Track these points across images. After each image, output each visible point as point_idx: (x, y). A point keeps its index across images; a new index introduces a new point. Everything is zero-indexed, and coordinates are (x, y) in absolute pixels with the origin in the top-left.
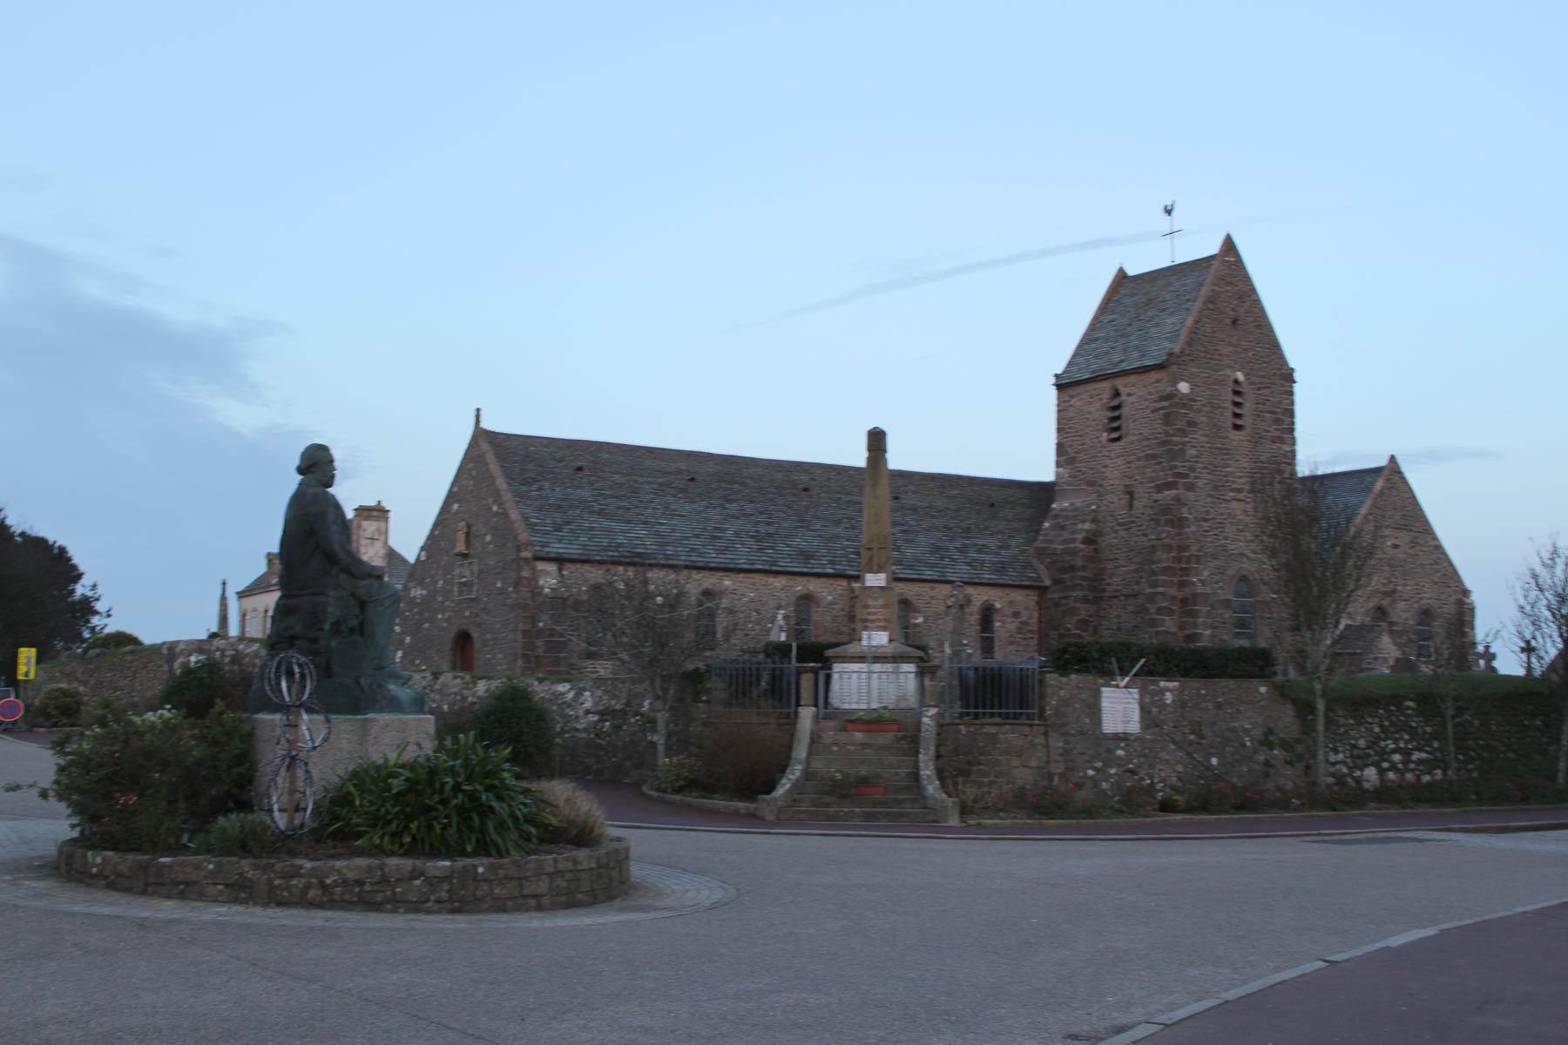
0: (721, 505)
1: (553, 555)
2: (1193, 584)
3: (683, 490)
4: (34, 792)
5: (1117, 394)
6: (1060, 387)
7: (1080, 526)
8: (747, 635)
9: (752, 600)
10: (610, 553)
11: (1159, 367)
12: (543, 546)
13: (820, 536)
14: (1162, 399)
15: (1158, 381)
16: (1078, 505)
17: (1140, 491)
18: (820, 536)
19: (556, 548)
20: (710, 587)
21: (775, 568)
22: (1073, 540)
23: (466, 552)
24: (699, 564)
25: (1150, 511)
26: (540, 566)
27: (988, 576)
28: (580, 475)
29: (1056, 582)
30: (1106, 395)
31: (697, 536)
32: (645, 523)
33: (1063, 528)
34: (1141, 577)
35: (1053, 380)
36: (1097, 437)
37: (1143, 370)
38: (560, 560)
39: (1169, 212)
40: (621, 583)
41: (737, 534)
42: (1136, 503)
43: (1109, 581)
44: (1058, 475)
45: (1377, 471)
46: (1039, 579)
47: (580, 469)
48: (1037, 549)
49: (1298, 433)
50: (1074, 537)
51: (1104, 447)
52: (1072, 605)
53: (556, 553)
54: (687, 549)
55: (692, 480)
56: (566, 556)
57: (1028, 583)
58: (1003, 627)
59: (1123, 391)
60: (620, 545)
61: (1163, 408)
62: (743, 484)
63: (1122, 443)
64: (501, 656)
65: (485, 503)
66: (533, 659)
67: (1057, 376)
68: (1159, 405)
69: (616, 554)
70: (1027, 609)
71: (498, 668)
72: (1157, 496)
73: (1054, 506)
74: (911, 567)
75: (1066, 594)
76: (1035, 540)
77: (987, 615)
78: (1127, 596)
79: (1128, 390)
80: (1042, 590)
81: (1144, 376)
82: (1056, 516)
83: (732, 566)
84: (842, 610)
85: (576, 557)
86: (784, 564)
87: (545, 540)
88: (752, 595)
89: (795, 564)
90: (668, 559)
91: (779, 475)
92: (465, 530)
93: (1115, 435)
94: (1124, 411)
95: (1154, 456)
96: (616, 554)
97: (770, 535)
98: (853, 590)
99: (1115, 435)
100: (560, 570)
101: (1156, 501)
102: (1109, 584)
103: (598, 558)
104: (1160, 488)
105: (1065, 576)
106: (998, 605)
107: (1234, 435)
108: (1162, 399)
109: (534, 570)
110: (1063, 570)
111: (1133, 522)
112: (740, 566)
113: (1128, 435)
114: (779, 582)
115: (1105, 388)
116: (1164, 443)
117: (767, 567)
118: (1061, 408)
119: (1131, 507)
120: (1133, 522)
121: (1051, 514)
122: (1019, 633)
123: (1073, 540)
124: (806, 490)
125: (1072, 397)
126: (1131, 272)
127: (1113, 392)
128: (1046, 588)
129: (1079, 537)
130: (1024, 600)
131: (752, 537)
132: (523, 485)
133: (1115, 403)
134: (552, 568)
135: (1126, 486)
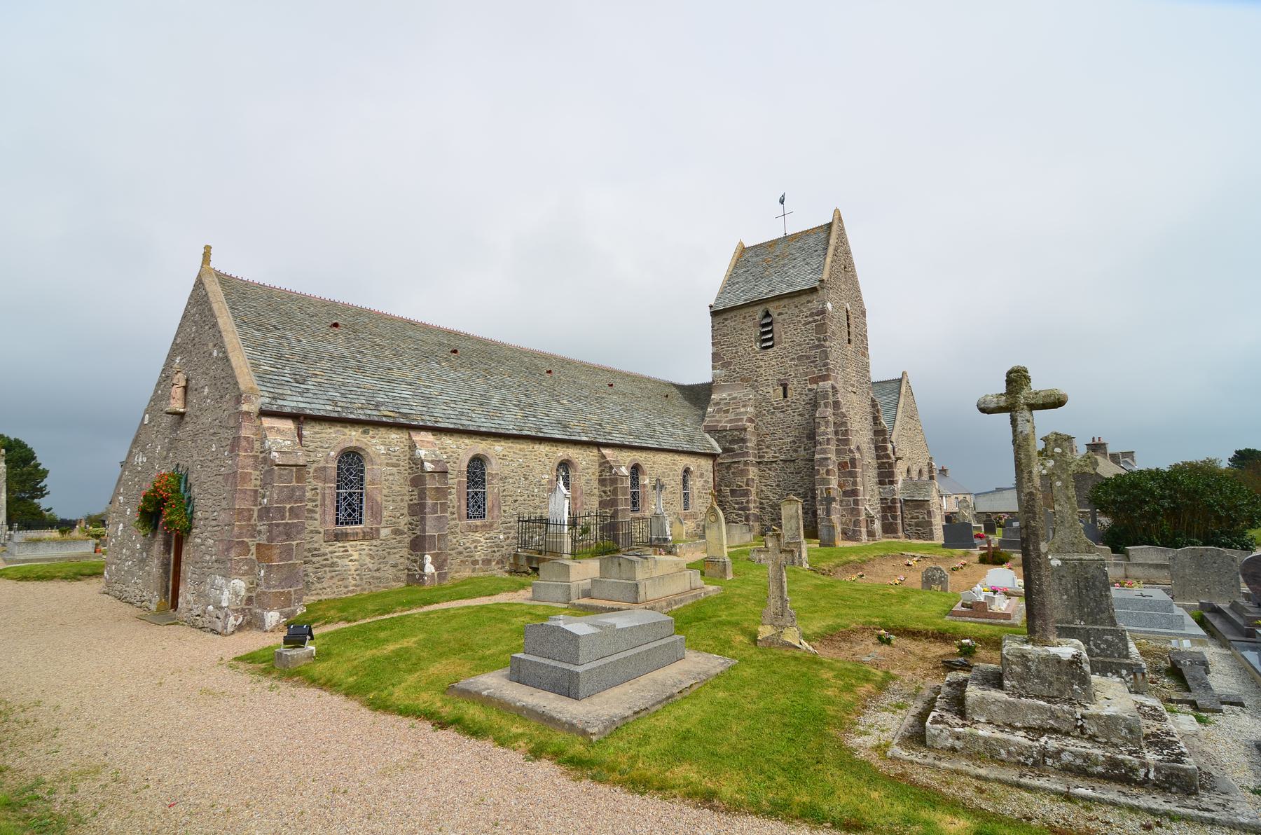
0: (484, 377)
1: (289, 410)
2: (851, 451)
3: (447, 360)
4: (615, 388)
5: (767, 315)
6: (715, 314)
7: (743, 410)
8: (515, 501)
9: (521, 466)
10: (369, 412)
11: (813, 290)
12: (274, 398)
13: (569, 409)
14: (812, 315)
15: (809, 302)
18: (569, 409)
19: (290, 405)
20: (481, 452)
21: (541, 435)
22: (741, 420)
23: (182, 410)
24: (471, 428)
25: (804, 397)
26: (267, 422)
27: (686, 446)
28: (336, 330)
29: (725, 450)
31: (466, 401)
32: (410, 384)
33: (727, 411)
34: (800, 447)
35: (708, 311)
36: (751, 347)
37: (792, 295)
38: (299, 418)
39: (782, 202)
40: (383, 447)
41: (503, 401)
42: (789, 393)
44: (715, 376)
45: (900, 380)
46: (712, 448)
47: (336, 325)
48: (705, 426)
49: (870, 352)
50: (739, 417)
51: (758, 353)
52: (742, 466)
53: (292, 408)
54: (457, 413)
55: (455, 351)
56: (308, 412)
57: (708, 451)
58: (696, 484)
59: (772, 311)
60: (383, 404)
61: (815, 321)
62: (499, 362)
63: (775, 348)
64: (211, 542)
65: (205, 349)
66: (253, 549)
67: (711, 307)
68: (811, 319)
69: (375, 413)
70: (707, 471)
71: (208, 558)
72: (815, 386)
73: (713, 397)
74: (638, 437)
75: (736, 460)
76: (703, 420)
77: (687, 471)
78: (785, 461)
80: (713, 456)
81: (796, 300)
82: (717, 404)
83: (503, 431)
84: (593, 474)
85: (323, 413)
86: (549, 432)
87: (280, 391)
88: (521, 460)
89: (557, 432)
90: (436, 422)
91: (526, 359)
92: (184, 384)
93: (770, 343)
94: (776, 327)
95: (808, 357)
96: (375, 413)
97: (531, 405)
98: (603, 456)
99: (770, 343)
100: (299, 430)
101: (809, 390)
102: (766, 453)
103: (351, 416)
104: (815, 380)
105: (735, 446)
106: (692, 469)
109: (259, 428)
110: (733, 442)
111: (788, 406)
112: (511, 432)
114: (543, 449)
115: (759, 312)
116: (818, 347)
117: (534, 434)
118: (716, 328)
119: (785, 396)
120: (788, 406)
121: (711, 402)
122: (703, 489)
123: (741, 420)
124: (550, 372)
125: (726, 319)
126: (746, 246)
127: (764, 314)
128: (719, 455)
129: (745, 418)
130: (707, 464)
131: (515, 405)
132: (258, 330)
133: (765, 321)
134: (289, 425)
135: (779, 380)
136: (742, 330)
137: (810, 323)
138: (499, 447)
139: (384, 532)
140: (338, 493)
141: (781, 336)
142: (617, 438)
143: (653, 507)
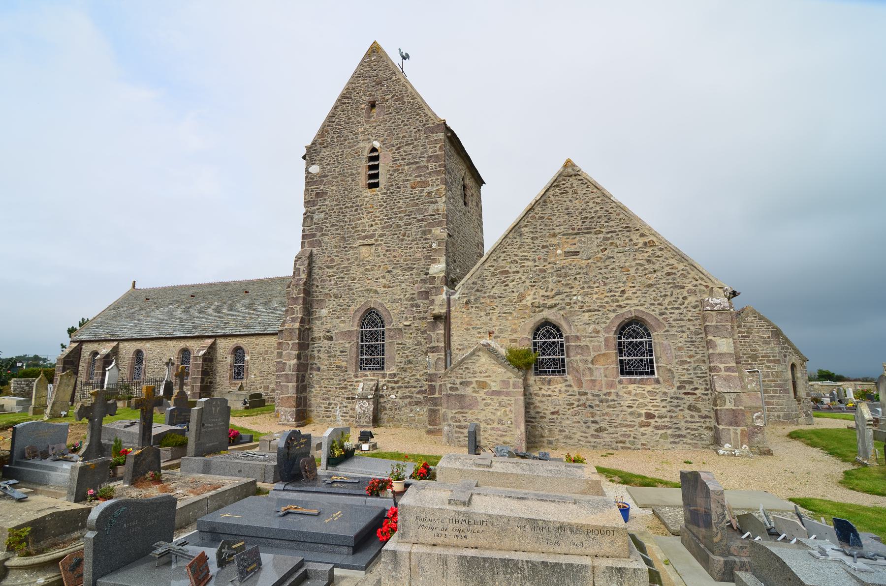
107: (369, 193)
138: (148, 345)
140: (361, 359)
143: (253, 376)
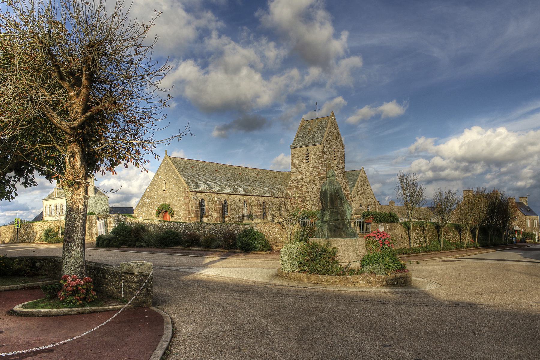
14: (320, 152)
16: (297, 178)
17: (314, 175)
30: (305, 151)
43: (63, 37)
68: (319, 154)
79: (311, 150)
95: (318, 167)
101: (319, 178)
108: (320, 152)
113: (311, 161)
129: (300, 186)
136: (300, 155)
137: (319, 155)
138: (230, 197)
139: (210, 216)
141: (311, 159)
142: (259, 194)
